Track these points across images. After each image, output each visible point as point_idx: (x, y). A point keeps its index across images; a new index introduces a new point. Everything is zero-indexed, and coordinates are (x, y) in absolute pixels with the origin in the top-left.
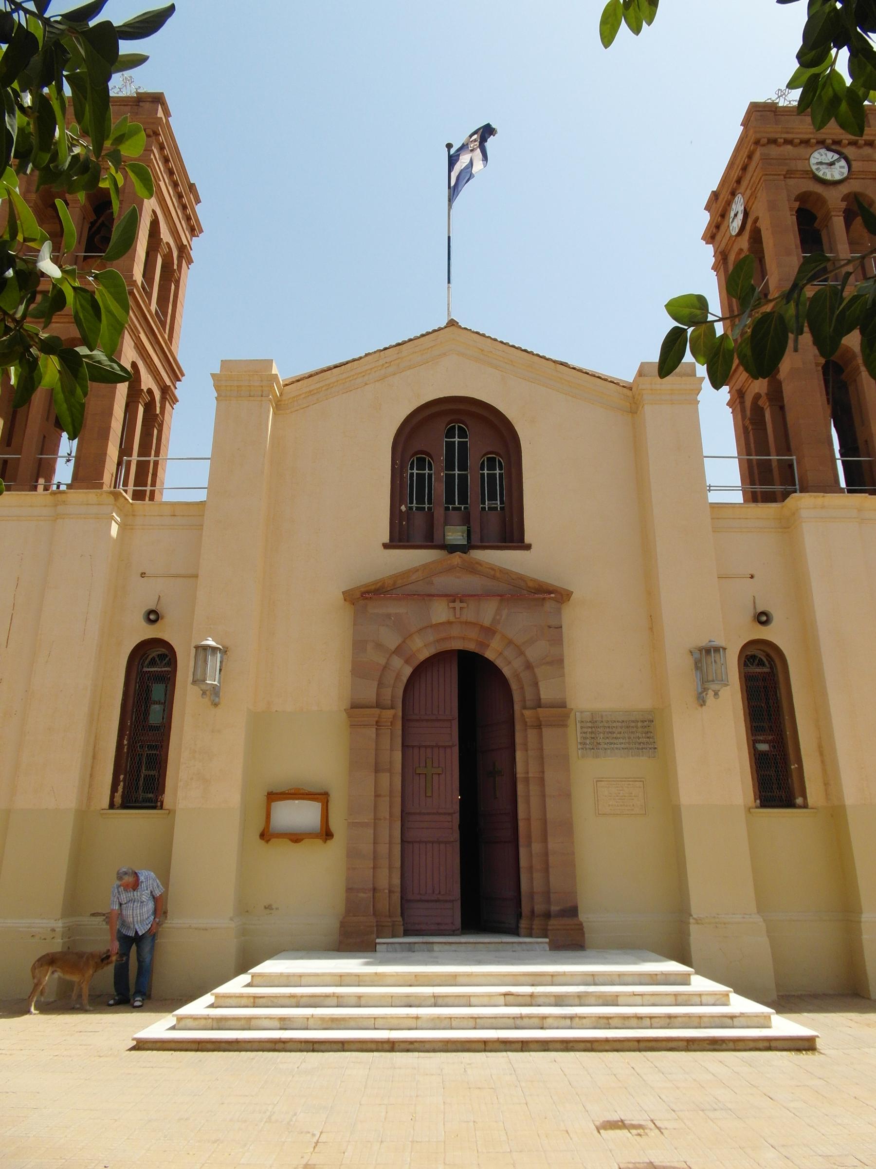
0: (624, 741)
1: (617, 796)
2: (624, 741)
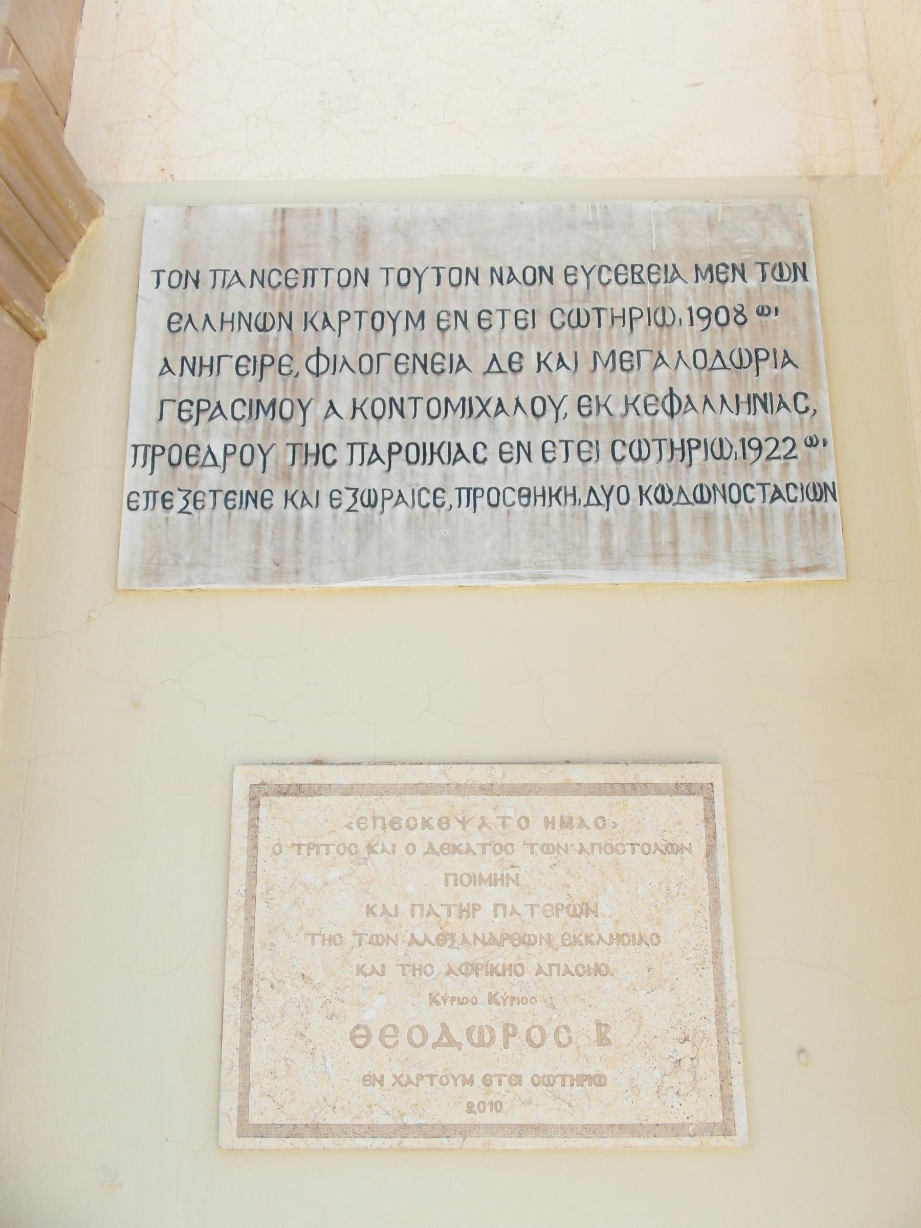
0: (542, 431)
1: (444, 938)
2: (542, 431)
